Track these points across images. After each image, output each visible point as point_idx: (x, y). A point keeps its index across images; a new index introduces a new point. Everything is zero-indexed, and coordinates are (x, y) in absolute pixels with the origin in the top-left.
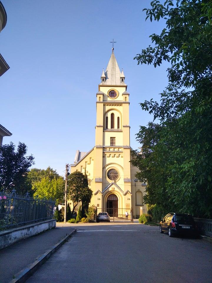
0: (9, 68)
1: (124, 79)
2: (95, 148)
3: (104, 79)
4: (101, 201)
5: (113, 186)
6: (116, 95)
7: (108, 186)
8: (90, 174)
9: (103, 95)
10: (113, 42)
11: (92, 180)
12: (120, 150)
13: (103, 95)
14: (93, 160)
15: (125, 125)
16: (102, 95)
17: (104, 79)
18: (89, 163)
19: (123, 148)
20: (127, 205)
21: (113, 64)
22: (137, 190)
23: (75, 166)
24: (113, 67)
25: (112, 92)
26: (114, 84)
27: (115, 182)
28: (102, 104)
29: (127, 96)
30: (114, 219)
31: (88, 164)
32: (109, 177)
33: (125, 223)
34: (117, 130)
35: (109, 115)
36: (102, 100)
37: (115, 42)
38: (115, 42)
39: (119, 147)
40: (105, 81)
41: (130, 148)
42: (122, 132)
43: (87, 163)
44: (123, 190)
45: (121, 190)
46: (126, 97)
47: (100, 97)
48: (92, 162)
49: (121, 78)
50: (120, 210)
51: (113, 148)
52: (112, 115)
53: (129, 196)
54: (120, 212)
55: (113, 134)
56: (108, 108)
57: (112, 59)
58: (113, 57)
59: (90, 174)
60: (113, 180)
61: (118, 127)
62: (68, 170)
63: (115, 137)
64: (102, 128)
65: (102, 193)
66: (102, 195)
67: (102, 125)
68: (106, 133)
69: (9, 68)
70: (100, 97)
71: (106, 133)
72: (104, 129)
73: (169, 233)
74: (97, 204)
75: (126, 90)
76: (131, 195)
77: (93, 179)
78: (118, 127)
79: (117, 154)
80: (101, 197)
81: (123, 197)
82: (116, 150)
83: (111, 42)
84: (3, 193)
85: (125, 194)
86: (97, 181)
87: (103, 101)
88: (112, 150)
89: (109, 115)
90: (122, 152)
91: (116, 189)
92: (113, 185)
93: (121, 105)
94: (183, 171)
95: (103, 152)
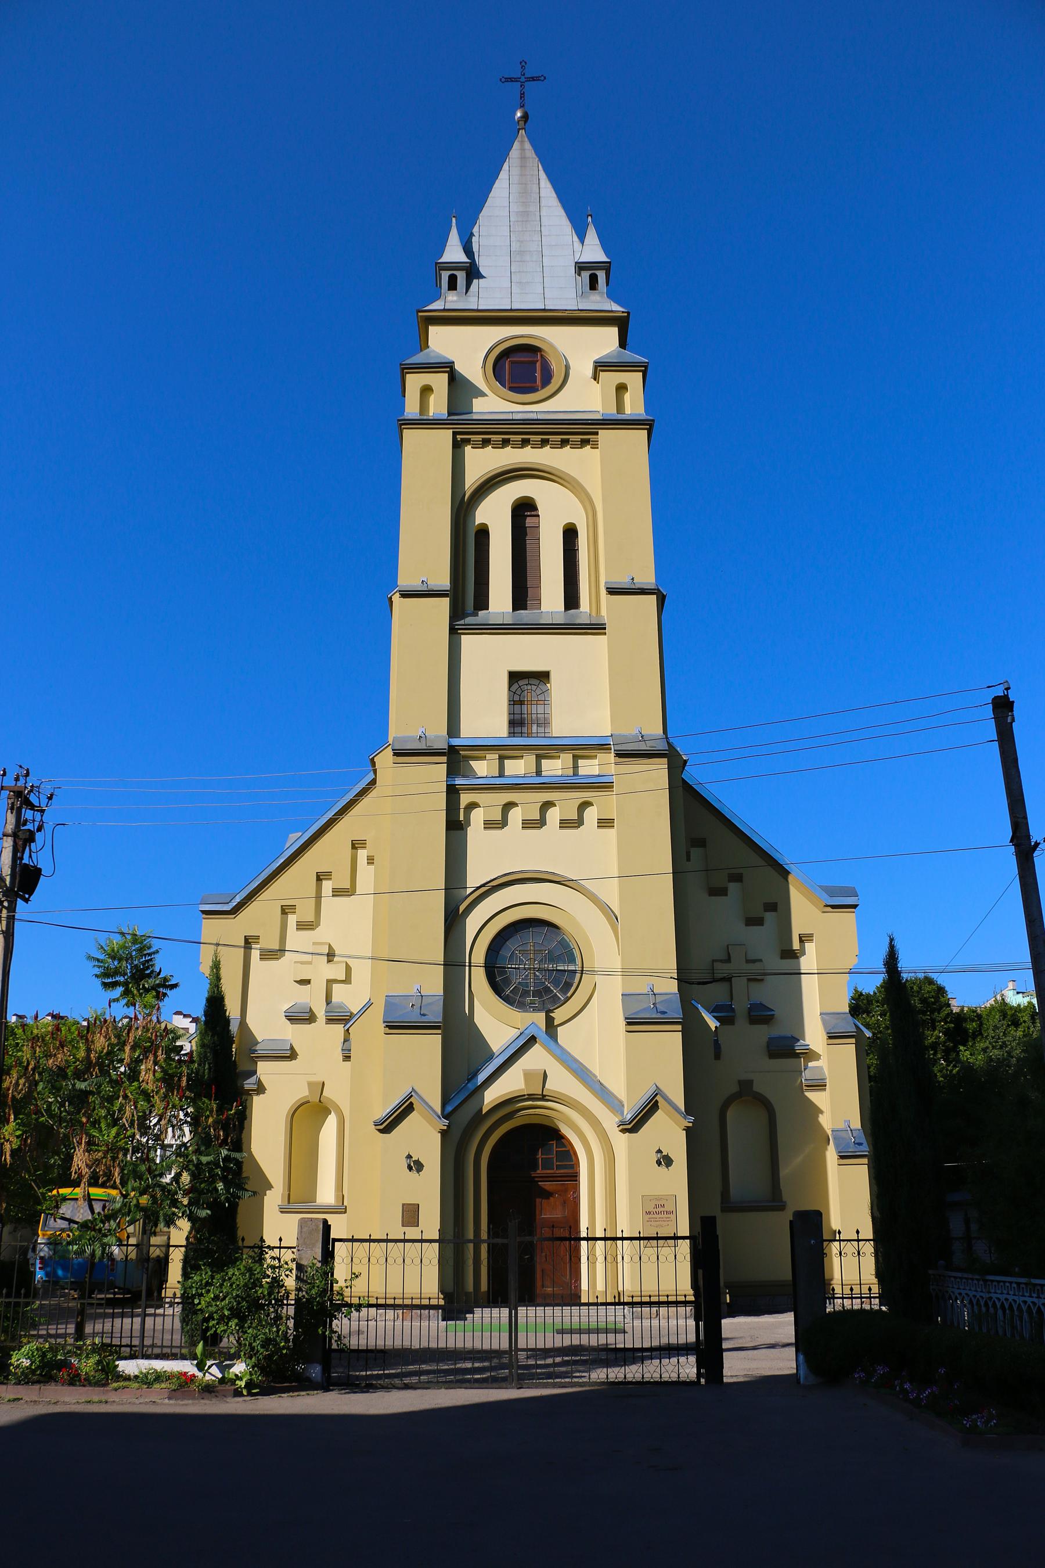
0: (753, 1080)
1: (601, 275)
3: (461, 276)
5: (536, 1058)
6: (547, 378)
7: (475, 1075)
8: (348, 969)
9: (454, 378)
12: (589, 768)
15: (622, 580)
16: (445, 377)
17: (461, 276)
19: (611, 757)
20: (656, 1209)
21: (522, 142)
22: (734, 1088)
23: (235, 911)
26: (531, 302)
27: (551, 1028)
28: (446, 436)
29: (634, 380)
31: (337, 893)
32: (497, 987)
33: (312, 827)
34: (560, 619)
36: (438, 406)
37: (533, 79)
38: (533, 79)
39: (582, 749)
42: (597, 628)
43: (327, 886)
44: (618, 1087)
45: (601, 1092)
46: (621, 388)
47: (426, 390)
48: (366, 876)
49: (581, 267)
51: (532, 758)
57: (515, 171)
58: (523, 158)
59: (348, 969)
60: (536, 1010)
61: (571, 600)
62: (30, 838)
63: (543, 676)
64: (446, 601)
66: (444, 1133)
67: (443, 580)
68: (468, 642)
69: (753, 1080)
71: (468, 642)
72: (456, 613)
74: (690, 861)
77: (369, 1005)
78: (571, 600)
79: (565, 805)
81: (621, 1141)
82: (555, 767)
85: (634, 1126)
86: (397, 1017)
87: (450, 414)
88: (518, 768)
91: (561, 1082)
92: (536, 1049)
93: (584, 443)
94: (115, 1221)
95: (452, 792)
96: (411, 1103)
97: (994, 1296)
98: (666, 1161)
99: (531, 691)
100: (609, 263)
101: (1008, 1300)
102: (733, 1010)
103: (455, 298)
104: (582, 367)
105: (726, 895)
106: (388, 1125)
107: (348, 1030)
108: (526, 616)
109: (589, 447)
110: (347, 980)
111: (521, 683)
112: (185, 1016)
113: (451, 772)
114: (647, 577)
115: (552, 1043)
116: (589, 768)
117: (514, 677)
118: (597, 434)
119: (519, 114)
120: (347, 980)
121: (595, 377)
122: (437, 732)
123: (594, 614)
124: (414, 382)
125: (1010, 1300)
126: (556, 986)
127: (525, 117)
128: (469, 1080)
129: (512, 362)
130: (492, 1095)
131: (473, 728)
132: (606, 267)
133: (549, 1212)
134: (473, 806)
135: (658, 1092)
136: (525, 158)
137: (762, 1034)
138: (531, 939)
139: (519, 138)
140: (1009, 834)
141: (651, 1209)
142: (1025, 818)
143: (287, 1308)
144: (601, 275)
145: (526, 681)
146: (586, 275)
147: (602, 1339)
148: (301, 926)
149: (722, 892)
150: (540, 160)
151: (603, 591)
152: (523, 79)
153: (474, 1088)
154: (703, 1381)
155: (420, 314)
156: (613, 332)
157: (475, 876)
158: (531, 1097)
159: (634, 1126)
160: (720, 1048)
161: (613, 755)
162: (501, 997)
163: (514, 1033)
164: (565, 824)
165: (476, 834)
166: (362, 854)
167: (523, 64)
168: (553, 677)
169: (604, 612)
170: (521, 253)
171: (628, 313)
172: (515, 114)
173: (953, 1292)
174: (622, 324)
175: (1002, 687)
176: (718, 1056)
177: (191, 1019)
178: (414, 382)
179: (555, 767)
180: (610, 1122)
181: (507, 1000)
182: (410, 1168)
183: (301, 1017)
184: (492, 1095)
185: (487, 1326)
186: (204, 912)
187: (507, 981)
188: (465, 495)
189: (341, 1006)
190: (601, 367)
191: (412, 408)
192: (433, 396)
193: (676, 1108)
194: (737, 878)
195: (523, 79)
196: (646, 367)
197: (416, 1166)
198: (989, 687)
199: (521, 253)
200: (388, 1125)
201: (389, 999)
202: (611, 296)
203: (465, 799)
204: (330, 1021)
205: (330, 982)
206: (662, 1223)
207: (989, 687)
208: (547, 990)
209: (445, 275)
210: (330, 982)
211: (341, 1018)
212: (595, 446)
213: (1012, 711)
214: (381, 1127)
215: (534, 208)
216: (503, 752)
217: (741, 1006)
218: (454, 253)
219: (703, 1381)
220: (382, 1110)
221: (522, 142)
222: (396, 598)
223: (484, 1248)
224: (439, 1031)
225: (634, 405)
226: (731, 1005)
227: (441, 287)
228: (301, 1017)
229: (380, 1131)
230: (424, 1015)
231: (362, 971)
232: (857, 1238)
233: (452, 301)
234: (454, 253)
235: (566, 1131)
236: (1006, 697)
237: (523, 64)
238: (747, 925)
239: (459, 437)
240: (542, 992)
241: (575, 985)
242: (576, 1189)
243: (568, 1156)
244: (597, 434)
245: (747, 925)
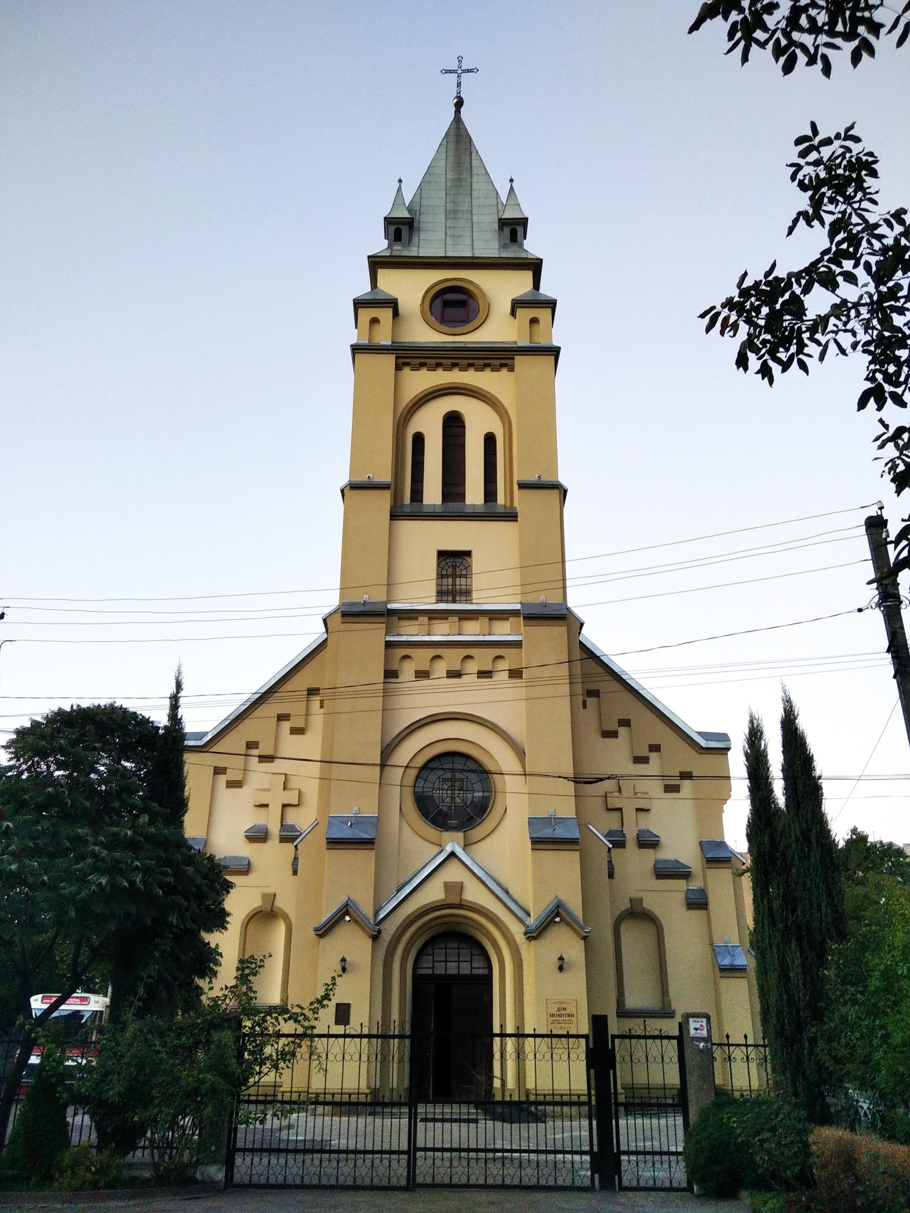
8: (300, 794)
10: (460, 71)
13: (396, 314)
15: (533, 478)
18: (300, 724)
22: (626, 905)
24: (459, 179)
25: (458, 312)
26: (463, 251)
37: (468, 71)
38: (468, 71)
40: (410, 240)
42: (510, 516)
50: (402, 1026)
59: (300, 794)
63: (468, 554)
73: (157, 805)
78: (490, 493)
91: (474, 894)
102: (624, 836)
103: (399, 248)
105: (617, 737)
107: (296, 846)
108: (454, 506)
117: (442, 554)
121: (513, 313)
123: (508, 505)
125: (865, 1108)
137: (649, 857)
140: (886, 644)
141: (554, 1012)
142: (902, 627)
146: (507, 231)
149: (613, 734)
151: (516, 486)
152: (459, 71)
160: (613, 869)
167: (460, 59)
168: (473, 554)
169: (516, 504)
175: (876, 507)
176: (611, 875)
180: (517, 930)
185: (361, 1133)
190: (517, 304)
195: (459, 71)
198: (862, 507)
204: (283, 839)
206: (564, 1025)
207: (862, 507)
211: (289, 836)
212: (511, 369)
213: (886, 527)
215: (465, 175)
217: (630, 834)
226: (622, 831)
228: (258, 836)
232: (744, 1043)
236: (880, 517)
238: (634, 763)
241: (489, 810)
244: (513, 359)
245: (634, 763)
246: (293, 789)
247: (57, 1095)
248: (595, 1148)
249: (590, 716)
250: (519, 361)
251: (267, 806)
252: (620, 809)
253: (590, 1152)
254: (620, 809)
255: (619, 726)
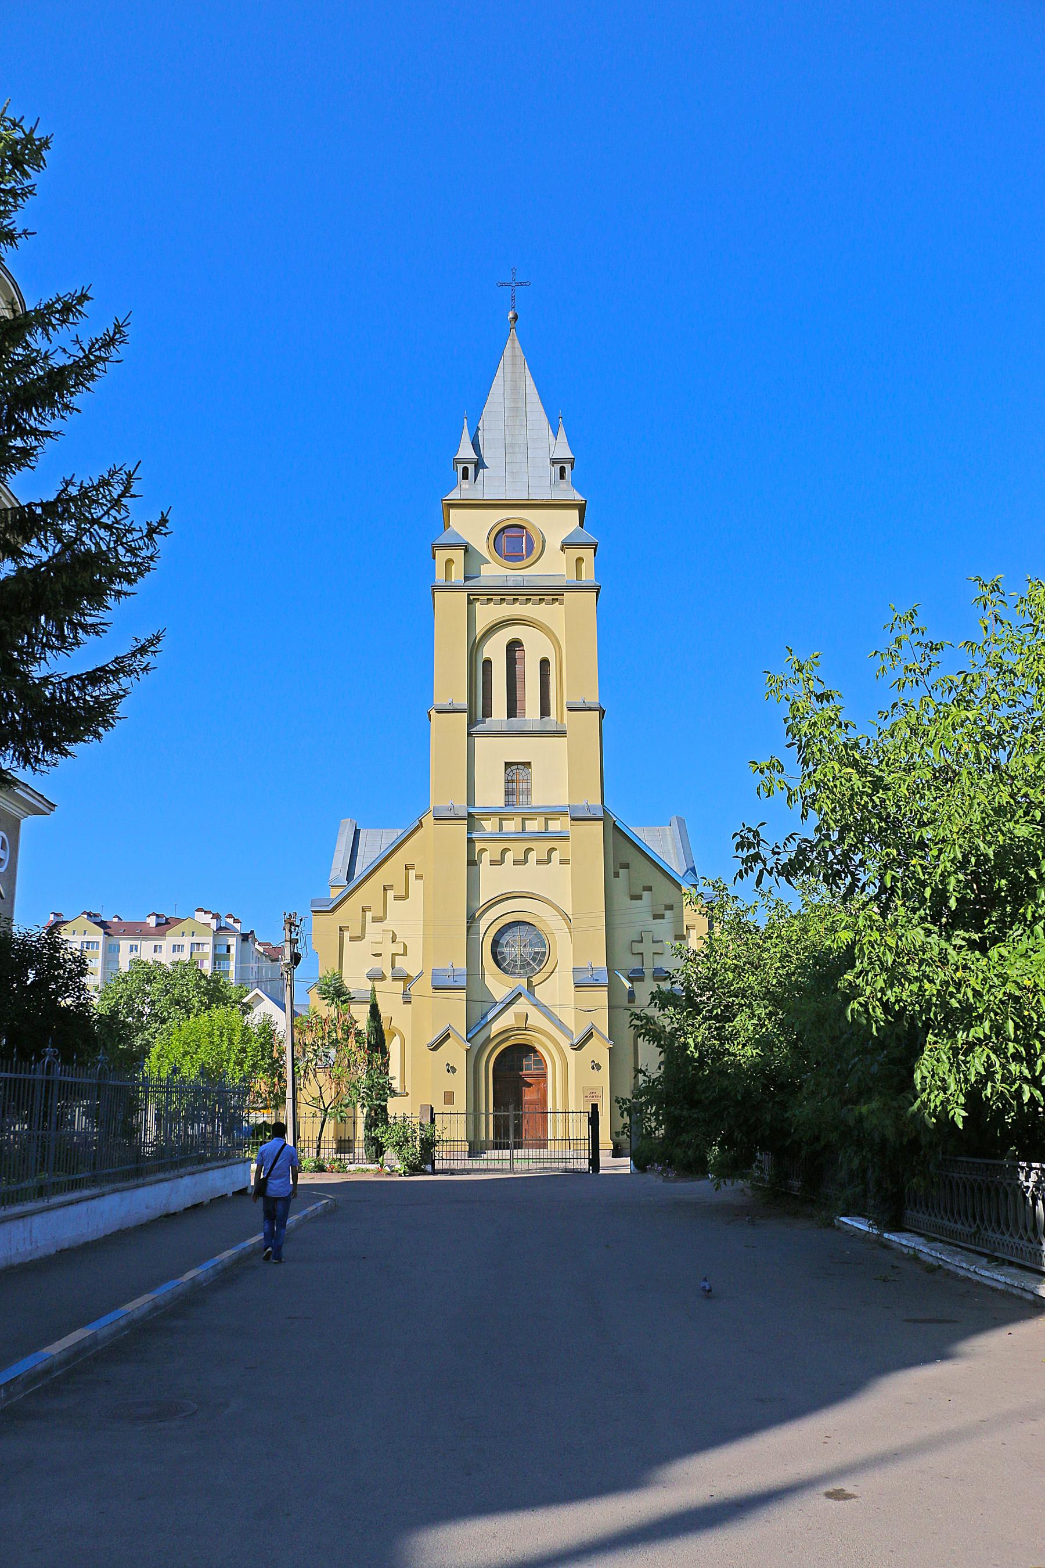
1: (568, 467)
2: (428, 820)
3: (471, 468)
4: (459, 1085)
5: (522, 1005)
7: (486, 1015)
8: (405, 946)
9: (467, 549)
11: (419, 976)
12: (555, 826)
13: (466, 551)
14: (419, 877)
17: (471, 468)
24: (515, 409)
28: (464, 596)
30: (511, 1159)
34: (537, 727)
35: (495, 650)
36: (457, 576)
39: (550, 814)
41: (606, 818)
42: (562, 733)
43: (390, 894)
44: (570, 1022)
45: (560, 1025)
46: (579, 560)
47: (449, 562)
52: (514, 646)
53: (599, 1050)
54: (554, 1128)
55: (517, 749)
56: (487, 614)
57: (508, 369)
58: (514, 356)
59: (405, 946)
61: (545, 711)
62: (297, 941)
65: (468, 1041)
67: (463, 702)
70: (449, 562)
72: (472, 723)
75: (581, 524)
76: (610, 1044)
78: (545, 711)
79: (540, 850)
80: (461, 1063)
81: (571, 1055)
82: (534, 826)
83: (503, 284)
84: (12, 1065)
85: (579, 1047)
87: (466, 579)
88: (511, 826)
89: (495, 650)
90: (567, 839)
91: (537, 1019)
92: (522, 1000)
95: (470, 841)
96: (449, 1034)
97: (950, 1174)
98: (597, 1067)
99: (519, 774)
100: (574, 459)
101: (994, 1182)
104: (554, 542)
106: (435, 1047)
109: (557, 603)
110: (405, 954)
111: (512, 768)
112: (206, 912)
113: (470, 829)
114: (593, 699)
115: (531, 996)
116: (555, 826)
118: (563, 595)
119: (511, 315)
120: (405, 954)
122: (461, 806)
124: (442, 556)
126: (534, 962)
127: (515, 318)
128: (482, 1019)
129: (507, 537)
130: (496, 1028)
131: (482, 801)
132: (572, 462)
133: (529, 1095)
134: (484, 850)
135: (593, 1027)
136: (515, 356)
138: (518, 933)
139: (511, 337)
143: (539, 1006)
144: (568, 467)
145: (516, 767)
146: (558, 467)
147: (562, 1165)
148: (375, 920)
150: (526, 359)
151: (565, 709)
153: (484, 1023)
154: (591, 1172)
155: (444, 502)
156: (575, 513)
157: (485, 895)
158: (519, 1029)
159: (579, 1047)
161: (569, 819)
162: (500, 968)
163: (508, 991)
164: (539, 862)
165: (484, 867)
166: (412, 873)
167: (514, 270)
168: (532, 764)
170: (512, 445)
171: (586, 501)
172: (508, 315)
173: (953, 1177)
174: (582, 508)
177: (211, 916)
178: (442, 556)
179: (534, 826)
180: (565, 1043)
181: (504, 970)
182: (448, 1071)
183: (376, 977)
184: (496, 1028)
186: (313, 911)
187: (504, 959)
188: (476, 638)
189: (401, 970)
191: (440, 578)
192: (454, 566)
193: (604, 1037)
194: (649, 889)
196: (596, 545)
197: (452, 1070)
199: (512, 445)
200: (435, 1047)
201: (434, 971)
202: (575, 485)
203: (478, 846)
204: (394, 979)
205: (394, 955)
208: (529, 964)
209: (460, 467)
210: (394, 955)
214: (431, 1048)
215: (521, 404)
216: (502, 816)
218: (466, 451)
219: (591, 1172)
220: (432, 1038)
221: (513, 340)
222: (433, 713)
223: (491, 1117)
224: (465, 991)
225: (588, 575)
227: (457, 471)
229: (430, 1049)
230: (456, 981)
231: (416, 949)
233: (464, 490)
234: (466, 451)
235: (538, 1048)
237: (514, 270)
239: (472, 597)
240: (526, 965)
242: (546, 1082)
243: (541, 1062)
246: (398, 942)
247: (994, 1108)
248: (591, 1157)
249: (621, 884)
250: (567, 595)
251: (381, 955)
252: (642, 954)
253: (589, 1158)
254: (642, 954)
255: (643, 891)
